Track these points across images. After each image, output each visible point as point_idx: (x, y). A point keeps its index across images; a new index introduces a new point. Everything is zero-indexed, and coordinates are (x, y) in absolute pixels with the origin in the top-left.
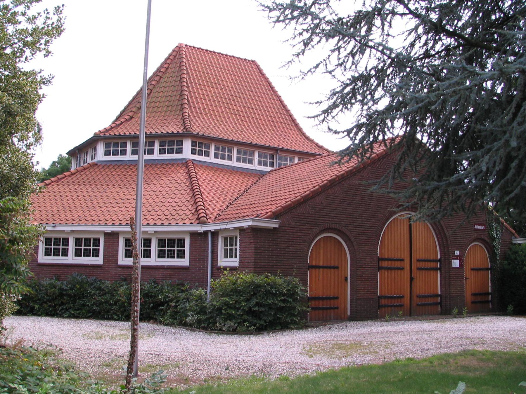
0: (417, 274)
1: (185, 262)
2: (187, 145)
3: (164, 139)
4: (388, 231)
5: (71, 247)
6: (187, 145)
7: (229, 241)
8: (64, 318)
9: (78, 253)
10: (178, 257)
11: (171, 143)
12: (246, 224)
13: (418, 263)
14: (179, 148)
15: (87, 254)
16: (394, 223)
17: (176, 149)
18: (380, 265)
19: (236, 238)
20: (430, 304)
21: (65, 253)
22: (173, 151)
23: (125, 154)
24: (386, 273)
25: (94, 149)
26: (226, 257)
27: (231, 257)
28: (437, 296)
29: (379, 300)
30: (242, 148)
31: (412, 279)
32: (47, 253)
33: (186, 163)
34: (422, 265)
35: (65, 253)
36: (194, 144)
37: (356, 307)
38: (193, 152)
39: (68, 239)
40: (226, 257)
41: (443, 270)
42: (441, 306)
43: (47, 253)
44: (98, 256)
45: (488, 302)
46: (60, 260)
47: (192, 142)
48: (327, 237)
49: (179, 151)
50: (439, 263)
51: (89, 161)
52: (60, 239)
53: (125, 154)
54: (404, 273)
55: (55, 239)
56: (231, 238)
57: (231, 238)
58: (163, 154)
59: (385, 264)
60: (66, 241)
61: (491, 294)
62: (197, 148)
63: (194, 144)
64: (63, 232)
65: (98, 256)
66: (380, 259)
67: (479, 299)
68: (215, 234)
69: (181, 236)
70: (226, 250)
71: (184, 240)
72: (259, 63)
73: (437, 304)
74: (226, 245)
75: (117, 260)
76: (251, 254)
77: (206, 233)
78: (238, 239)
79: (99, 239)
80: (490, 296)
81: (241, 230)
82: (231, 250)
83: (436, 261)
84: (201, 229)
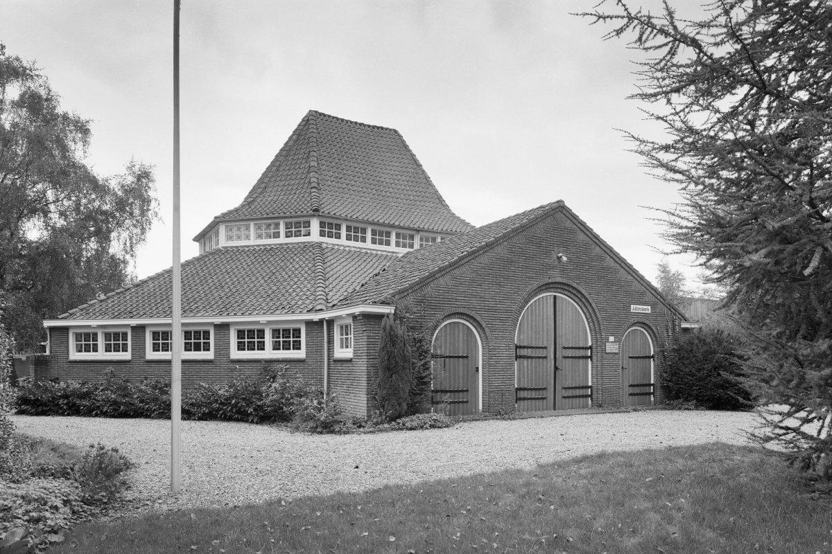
0: (563, 364)
1: (301, 354)
2: (315, 225)
3: (324, 220)
4: (528, 315)
5: (268, 339)
6: (315, 225)
7: (345, 329)
8: (153, 418)
9: (108, 349)
10: (85, 351)
11: (298, 225)
12: (357, 310)
13: (564, 350)
14: (298, 231)
15: (197, 348)
16: (539, 302)
17: (295, 232)
18: (518, 354)
19: (351, 325)
20: (579, 397)
21: (261, 347)
22: (338, 233)
23: (279, 237)
24: (525, 362)
25: (217, 234)
26: (342, 347)
27: (347, 347)
28: (587, 387)
29: (516, 392)
30: (377, 228)
31: (556, 368)
32: (241, 347)
33: (313, 245)
34: (570, 353)
35: (261, 347)
36: (322, 225)
37: (489, 401)
38: (322, 234)
39: (264, 330)
40: (342, 347)
41: (594, 358)
42: (592, 399)
43: (241, 347)
44: (208, 350)
45: (650, 394)
46: (291, 354)
47: (321, 223)
48: (454, 323)
49: (298, 233)
50: (589, 351)
51: (214, 247)
52: (200, 332)
53: (279, 237)
54: (547, 362)
55: (283, 330)
56: (347, 327)
57: (347, 327)
58: (289, 237)
59: (524, 352)
60: (261, 333)
61: (653, 385)
62: (327, 230)
63: (323, 225)
64: (258, 323)
65: (208, 350)
66: (517, 347)
67: (637, 390)
68: (330, 322)
69: (206, 328)
70: (342, 339)
71: (299, 330)
72: (401, 133)
73: (587, 396)
74: (342, 335)
75: (228, 354)
76: (364, 343)
77: (321, 322)
78: (352, 327)
79: (209, 332)
80: (652, 387)
81: (354, 317)
82: (347, 339)
83: (586, 348)
84: (316, 317)
